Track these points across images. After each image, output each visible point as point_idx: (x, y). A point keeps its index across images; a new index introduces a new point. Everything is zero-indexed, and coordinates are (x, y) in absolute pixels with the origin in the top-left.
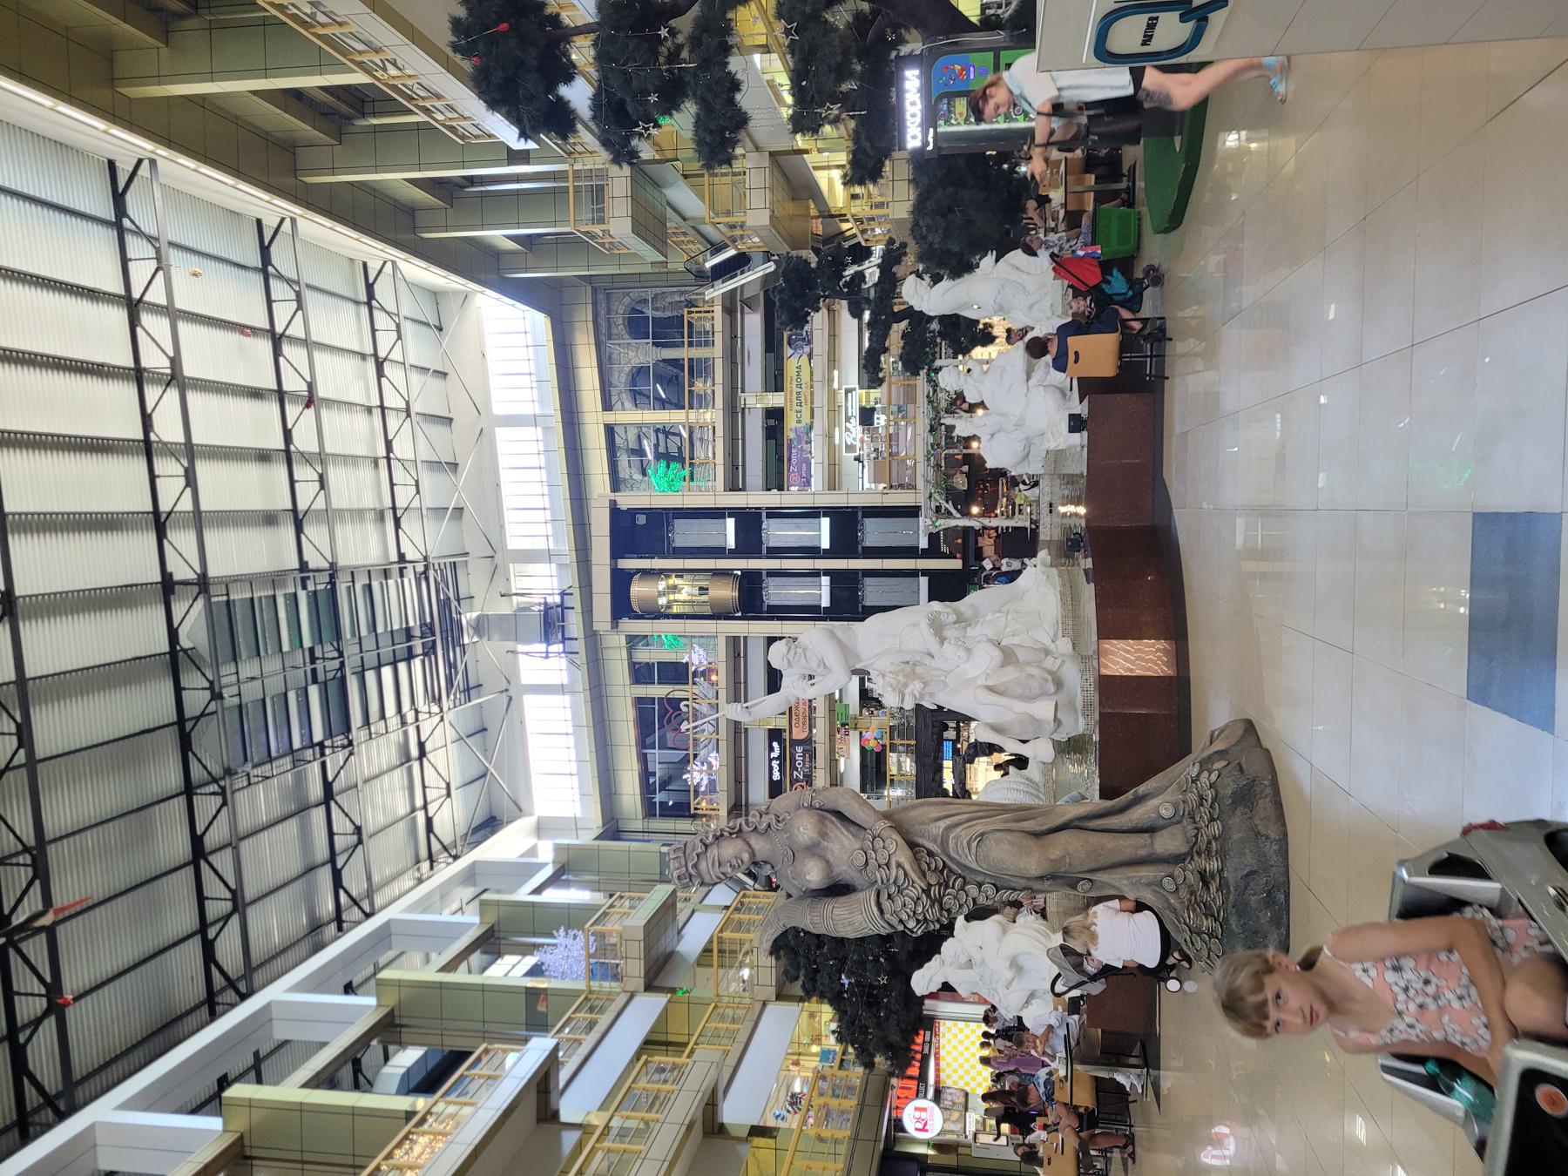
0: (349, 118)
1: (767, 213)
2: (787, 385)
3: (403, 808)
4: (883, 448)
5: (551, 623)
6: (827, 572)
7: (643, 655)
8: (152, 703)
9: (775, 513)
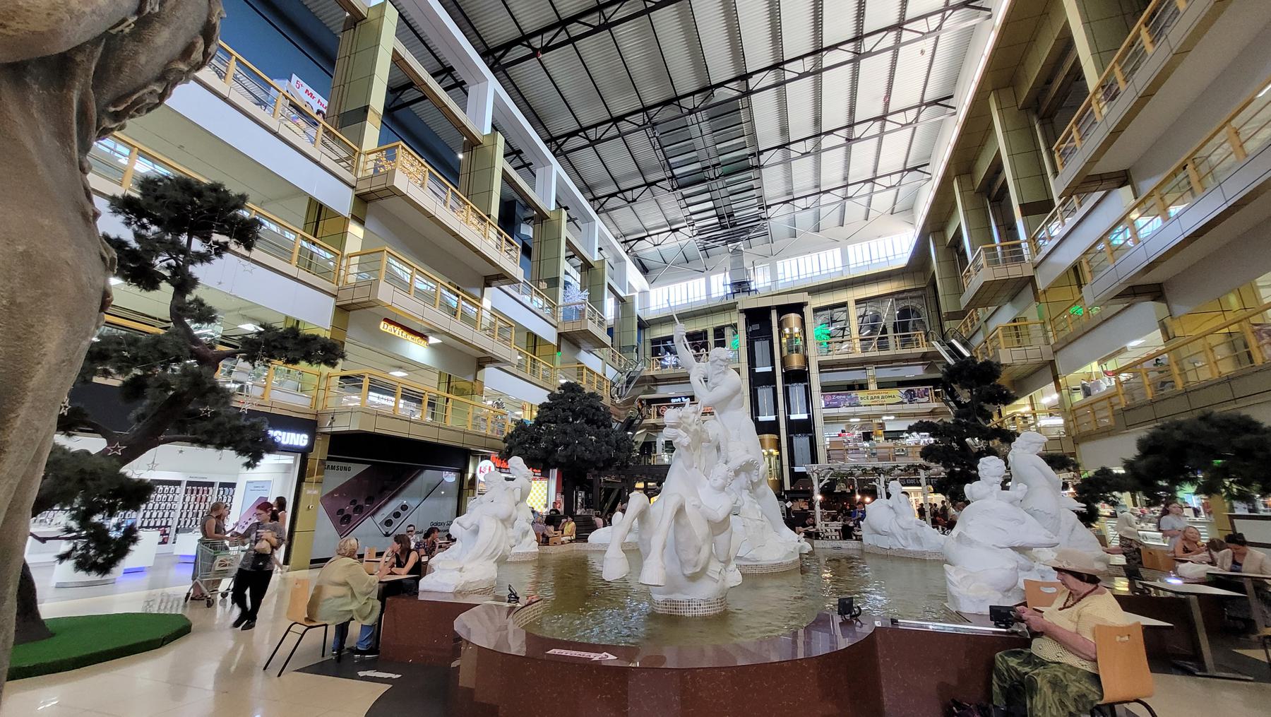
0: (1037, 112)
1: (1009, 361)
2: (882, 391)
3: (647, 225)
4: (851, 445)
5: (741, 286)
6: (777, 419)
7: (728, 332)
8: (686, 81)
9: (808, 391)
